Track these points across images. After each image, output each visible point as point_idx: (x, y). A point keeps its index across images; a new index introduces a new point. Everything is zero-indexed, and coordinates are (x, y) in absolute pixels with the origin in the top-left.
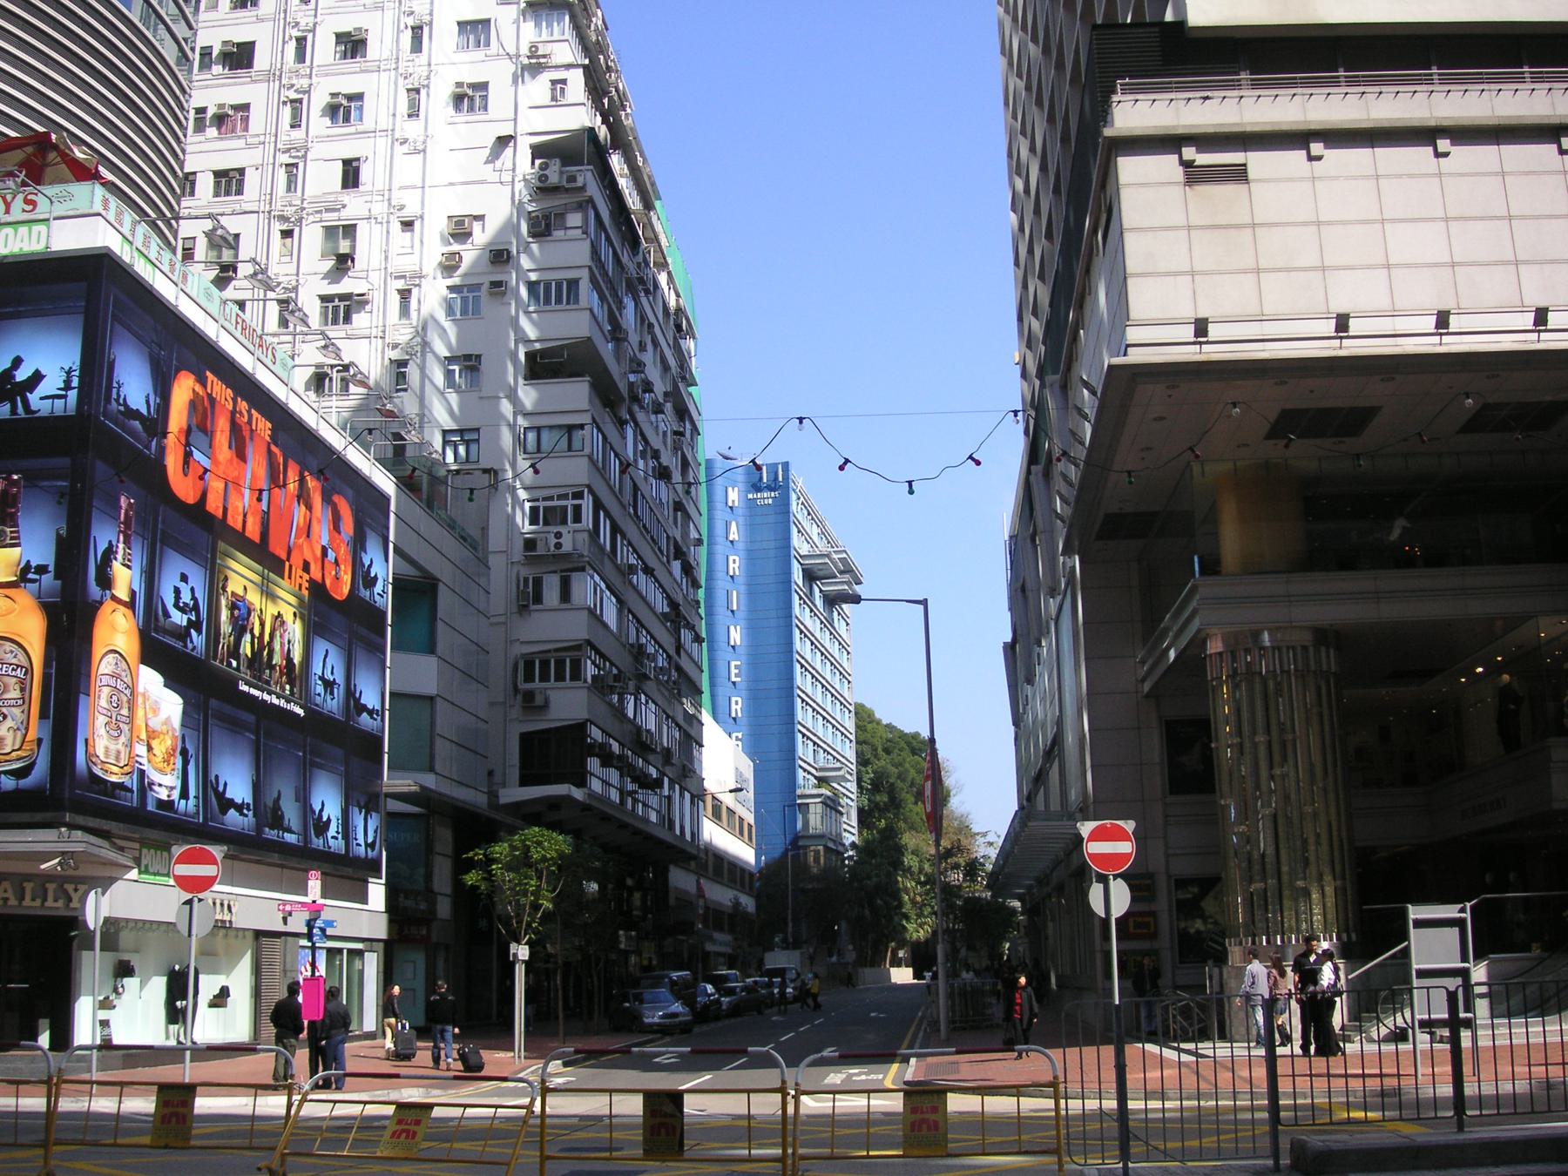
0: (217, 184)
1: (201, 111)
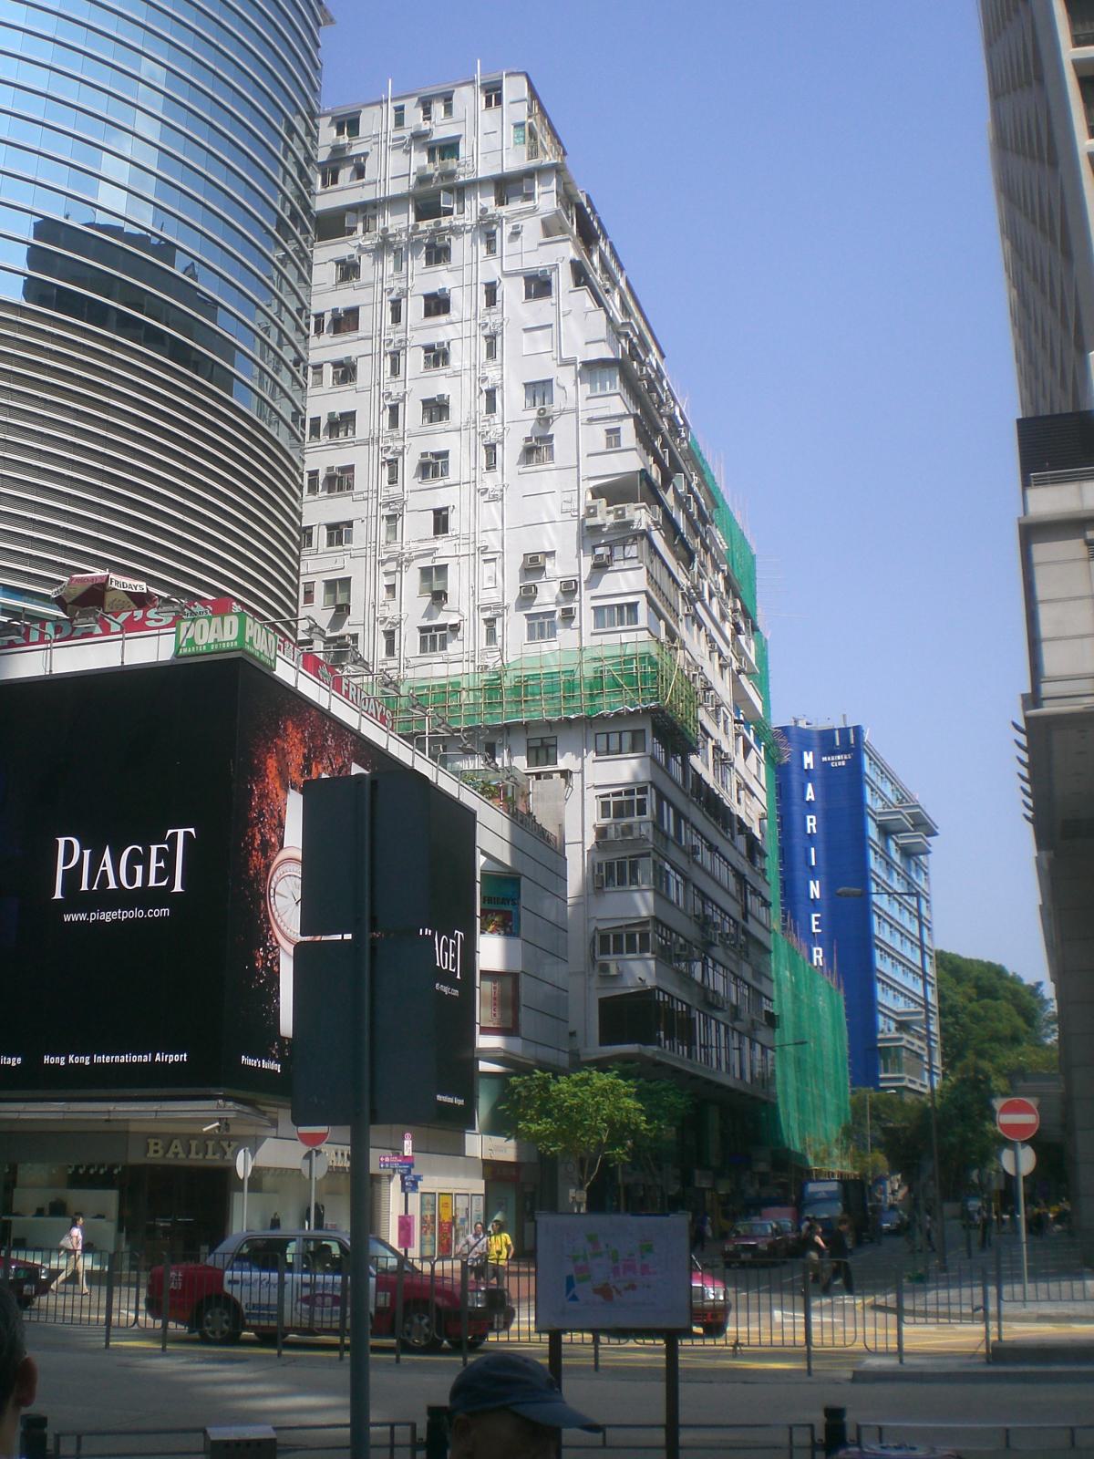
0: (330, 536)
1: (314, 474)
